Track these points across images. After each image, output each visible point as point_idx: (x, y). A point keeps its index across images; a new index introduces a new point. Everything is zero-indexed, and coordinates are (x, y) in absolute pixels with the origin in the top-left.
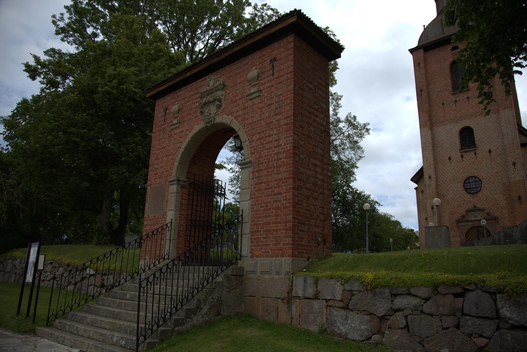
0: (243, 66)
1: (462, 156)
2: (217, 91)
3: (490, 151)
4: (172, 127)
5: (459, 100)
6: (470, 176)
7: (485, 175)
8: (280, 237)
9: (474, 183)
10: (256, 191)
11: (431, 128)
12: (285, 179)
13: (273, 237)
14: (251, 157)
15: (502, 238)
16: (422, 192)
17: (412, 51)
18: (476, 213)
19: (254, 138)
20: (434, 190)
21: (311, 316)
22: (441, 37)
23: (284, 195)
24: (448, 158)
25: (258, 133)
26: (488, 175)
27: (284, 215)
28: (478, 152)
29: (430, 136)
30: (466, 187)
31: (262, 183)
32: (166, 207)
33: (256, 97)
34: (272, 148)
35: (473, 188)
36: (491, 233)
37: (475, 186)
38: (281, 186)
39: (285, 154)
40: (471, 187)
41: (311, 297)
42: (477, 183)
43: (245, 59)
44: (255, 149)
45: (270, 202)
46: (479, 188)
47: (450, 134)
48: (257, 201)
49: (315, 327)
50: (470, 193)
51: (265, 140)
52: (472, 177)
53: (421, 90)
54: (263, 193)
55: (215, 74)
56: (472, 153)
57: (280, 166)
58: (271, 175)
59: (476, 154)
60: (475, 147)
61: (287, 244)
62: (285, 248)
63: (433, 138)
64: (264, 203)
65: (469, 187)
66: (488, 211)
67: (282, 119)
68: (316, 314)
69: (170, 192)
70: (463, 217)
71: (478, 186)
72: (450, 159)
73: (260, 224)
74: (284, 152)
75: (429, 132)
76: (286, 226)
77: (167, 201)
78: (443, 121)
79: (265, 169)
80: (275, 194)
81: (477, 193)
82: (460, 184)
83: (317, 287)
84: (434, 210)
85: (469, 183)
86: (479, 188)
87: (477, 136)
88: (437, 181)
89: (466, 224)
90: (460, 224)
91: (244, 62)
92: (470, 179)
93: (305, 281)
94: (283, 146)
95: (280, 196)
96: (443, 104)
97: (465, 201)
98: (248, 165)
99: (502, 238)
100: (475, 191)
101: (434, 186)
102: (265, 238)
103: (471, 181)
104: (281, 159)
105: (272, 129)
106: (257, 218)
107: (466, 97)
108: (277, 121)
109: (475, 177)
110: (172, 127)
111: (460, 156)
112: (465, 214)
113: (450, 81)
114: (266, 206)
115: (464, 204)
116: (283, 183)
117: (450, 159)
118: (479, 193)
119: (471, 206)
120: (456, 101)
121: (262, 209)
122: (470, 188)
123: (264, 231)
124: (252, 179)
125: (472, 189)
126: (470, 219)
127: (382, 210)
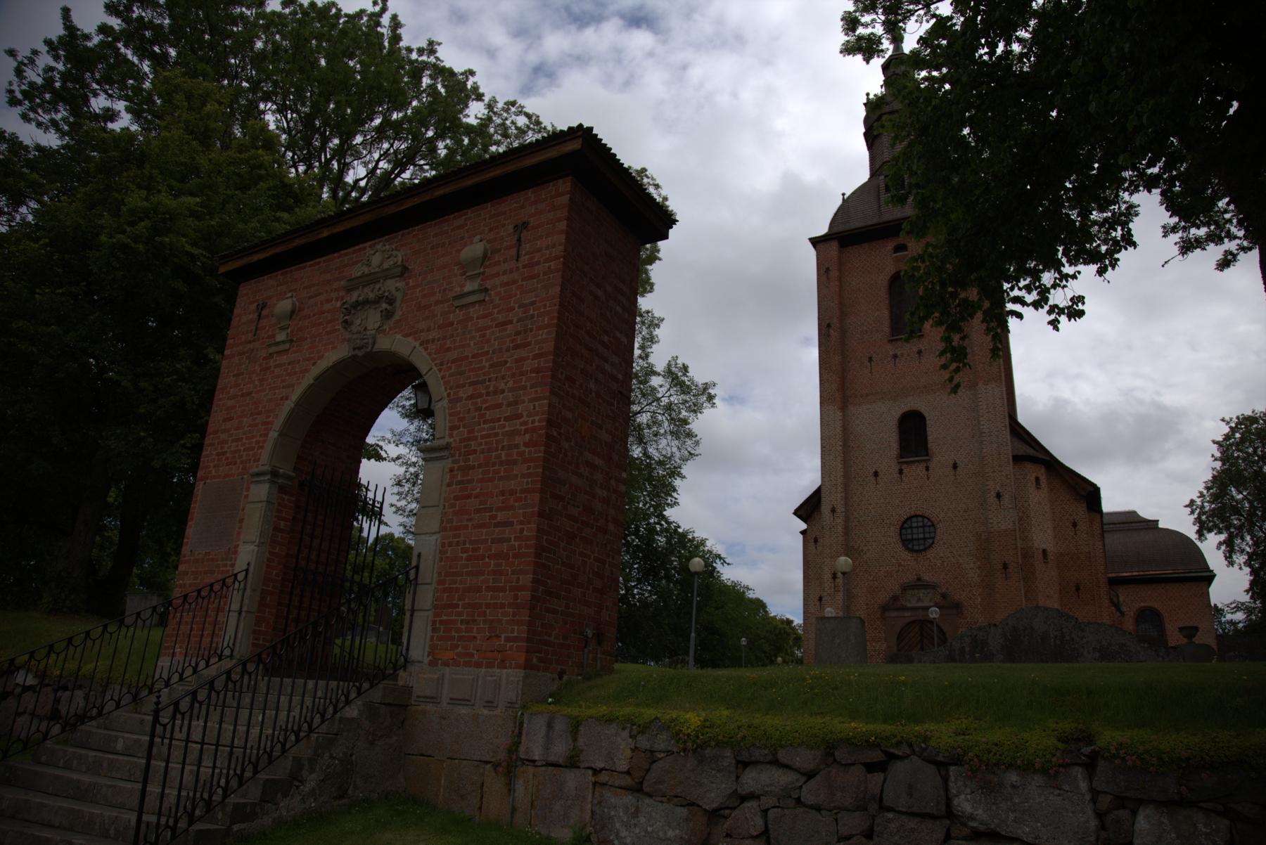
0: (453, 230)
1: (901, 472)
2: (386, 278)
3: (955, 466)
4: (273, 349)
8: (500, 621)
9: (921, 530)
11: (843, 408)
15: (967, 649)
16: (816, 541)
17: (815, 242)
22: (874, 221)
28: (931, 465)
31: (469, 497)
32: (239, 534)
33: (473, 304)
37: (921, 536)
41: (561, 761)
47: (878, 423)
52: (916, 516)
53: (829, 326)
56: (921, 466)
59: (927, 469)
62: (511, 647)
63: (845, 429)
65: (909, 537)
67: (528, 358)
70: (895, 598)
72: (876, 474)
74: (526, 431)
75: (839, 414)
76: (516, 597)
77: (241, 521)
80: (496, 525)
81: (925, 550)
83: (575, 740)
87: (933, 433)
88: (847, 519)
93: (550, 726)
94: (525, 418)
95: (507, 530)
96: (870, 359)
97: (900, 565)
99: (967, 649)
101: (840, 529)
104: (517, 446)
107: (915, 349)
110: (273, 349)
113: (886, 313)
114: (474, 550)
117: (876, 474)
120: (895, 356)
122: (912, 540)
124: (449, 485)
127: (729, 574)
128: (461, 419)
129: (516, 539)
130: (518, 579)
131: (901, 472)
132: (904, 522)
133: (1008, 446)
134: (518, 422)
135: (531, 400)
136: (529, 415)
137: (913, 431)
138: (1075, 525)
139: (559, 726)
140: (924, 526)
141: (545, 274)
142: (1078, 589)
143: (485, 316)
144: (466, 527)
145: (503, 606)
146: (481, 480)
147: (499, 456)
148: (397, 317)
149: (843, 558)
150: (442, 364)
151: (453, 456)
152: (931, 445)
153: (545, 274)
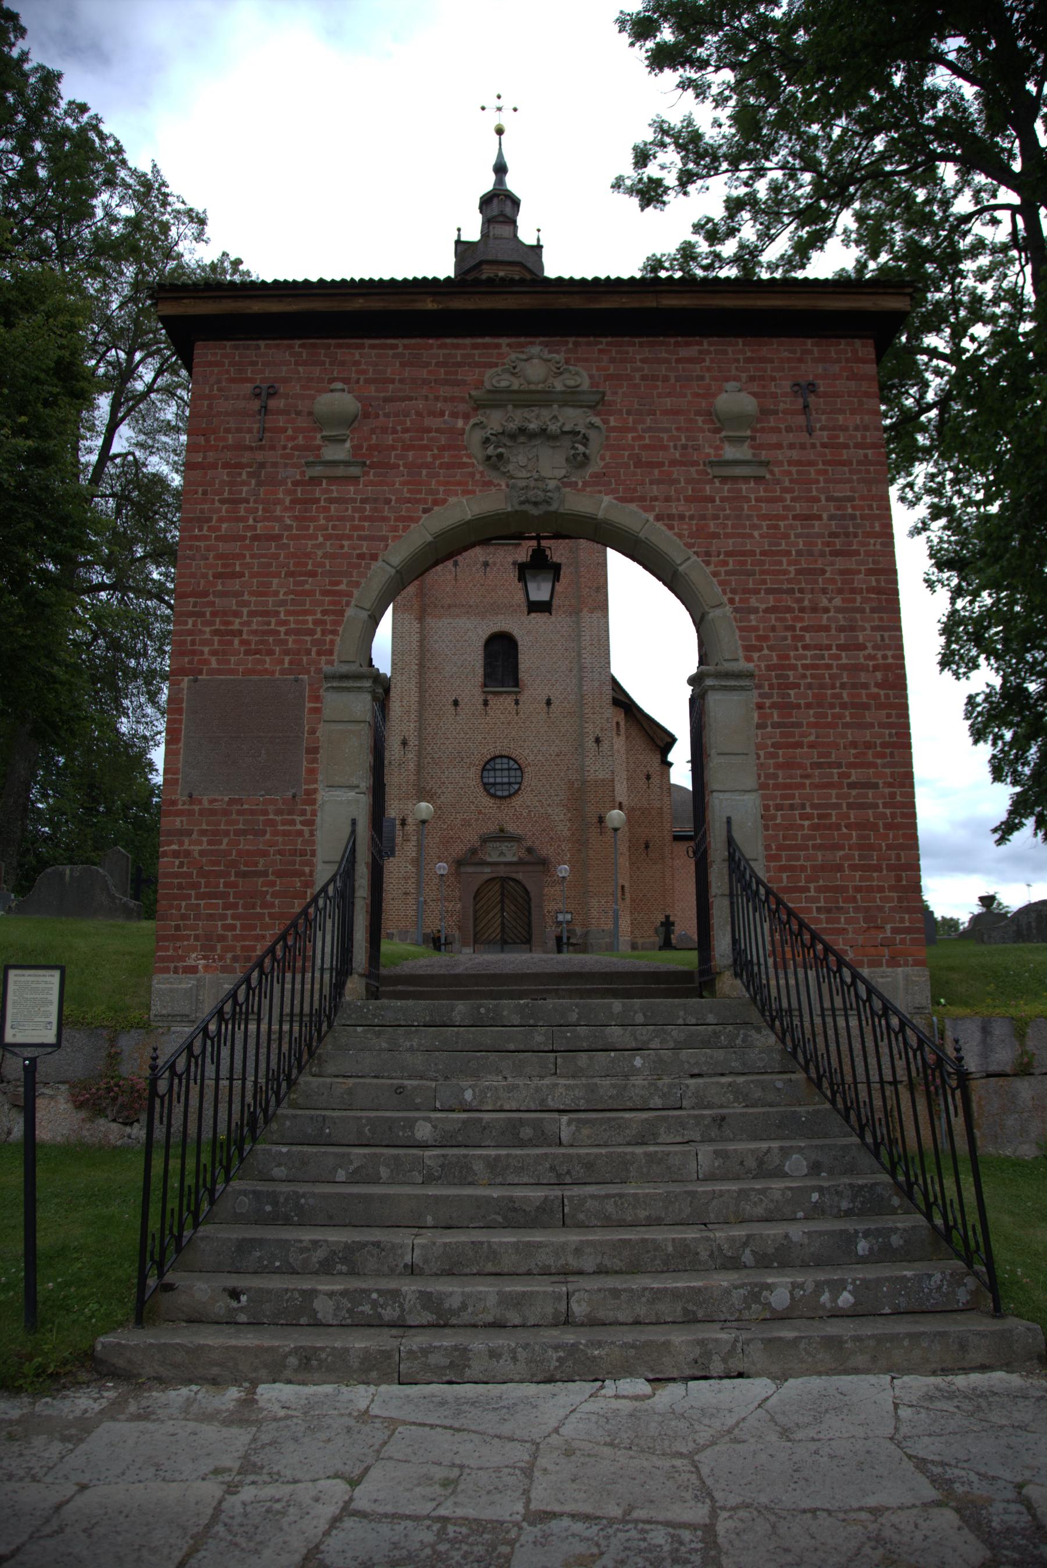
0: (678, 361)
1: (486, 703)
2: (564, 404)
3: (549, 703)
4: (317, 471)
5: (495, 564)
6: (497, 753)
7: (532, 757)
8: (880, 909)
9: (506, 773)
10: (778, 766)
11: (421, 619)
12: (884, 745)
13: (857, 909)
14: (749, 659)
15: (1034, 924)
18: (504, 847)
19: (753, 602)
20: (413, 777)
21: (1010, 1121)
23: (887, 790)
24: (451, 700)
25: (769, 591)
26: (540, 757)
27: (889, 847)
28: (522, 698)
29: (416, 637)
30: (485, 780)
31: (799, 745)
32: (312, 772)
33: (746, 479)
34: (829, 647)
35: (502, 784)
36: (532, 895)
37: (506, 780)
38: (873, 765)
39: (879, 675)
40: (499, 780)
41: (1008, 1069)
42: (512, 773)
43: (688, 344)
44: (765, 638)
45: (837, 806)
46: (516, 787)
48: (784, 797)
49: (1026, 1147)
50: (494, 796)
51: (802, 619)
52: (501, 756)
54: (807, 776)
55: (546, 345)
56: (510, 700)
57: (866, 707)
58: (832, 726)
59: (517, 703)
60: (517, 685)
61: (908, 931)
62: (903, 941)
64: (814, 806)
65: (492, 780)
66: (530, 844)
67: (859, 572)
68: (1026, 1115)
69: (327, 713)
70: (474, 851)
71: (512, 780)
72: (456, 703)
73: (803, 868)
74: (876, 668)
75: (416, 625)
76: (899, 879)
77: (313, 751)
78: (449, 607)
79: (808, 706)
80: (852, 786)
81: (510, 796)
82: (473, 769)
83: (1022, 1044)
84: (407, 828)
85: (495, 770)
86: (516, 787)
87: (526, 661)
88: (419, 756)
89: (479, 869)
90: (463, 869)
91: (684, 352)
92: (498, 761)
93: (985, 1030)
94: (869, 651)
95: (870, 792)
97: (480, 812)
98: (742, 683)
99: (1034, 924)
100: (506, 793)
101: (412, 766)
102: (828, 910)
103: (498, 766)
104: (865, 686)
105: (824, 591)
106: (791, 848)
108: (842, 572)
109: (509, 758)
110: (317, 471)
111: (481, 701)
112: (477, 845)
114: (820, 817)
115: (477, 820)
116: (883, 756)
118: (514, 799)
119: (492, 828)
120: (486, 564)
121: (806, 823)
122: (494, 784)
123: (819, 890)
124: (759, 726)
125: (498, 787)
126: (489, 860)
128: (765, 638)
129: (886, 805)
130: (898, 857)
131: (486, 703)
132: (487, 763)
133: (608, 689)
134: (862, 653)
135: (874, 629)
136: (876, 647)
137: (501, 657)
138: (648, 777)
139: (1000, 1030)
140: (509, 769)
141: (859, 463)
142: (647, 847)
143: (769, 500)
144: (802, 786)
145: (881, 889)
146: (816, 725)
147: (839, 696)
148: (596, 466)
149: (423, 804)
150: (708, 554)
151: (759, 687)
152: (521, 675)
153: (859, 463)
